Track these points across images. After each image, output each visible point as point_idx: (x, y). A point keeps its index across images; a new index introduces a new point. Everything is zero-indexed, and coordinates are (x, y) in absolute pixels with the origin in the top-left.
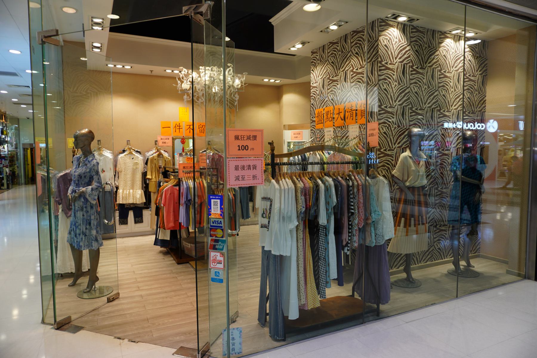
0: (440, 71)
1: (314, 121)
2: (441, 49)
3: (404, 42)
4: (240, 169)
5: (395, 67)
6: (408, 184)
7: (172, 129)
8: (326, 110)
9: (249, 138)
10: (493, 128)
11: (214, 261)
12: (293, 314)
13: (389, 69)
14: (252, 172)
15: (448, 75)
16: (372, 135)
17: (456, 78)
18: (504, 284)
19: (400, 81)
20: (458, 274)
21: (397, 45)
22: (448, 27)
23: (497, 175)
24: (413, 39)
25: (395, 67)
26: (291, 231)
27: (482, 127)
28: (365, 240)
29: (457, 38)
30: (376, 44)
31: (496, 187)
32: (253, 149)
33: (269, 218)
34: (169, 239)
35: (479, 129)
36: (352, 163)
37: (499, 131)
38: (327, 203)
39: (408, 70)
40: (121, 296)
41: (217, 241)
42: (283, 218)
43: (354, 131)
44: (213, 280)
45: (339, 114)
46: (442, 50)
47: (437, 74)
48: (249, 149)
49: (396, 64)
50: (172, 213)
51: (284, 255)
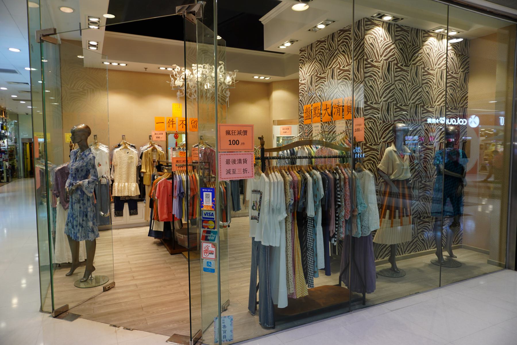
0: (424, 68)
1: (303, 117)
2: (424, 47)
3: (389, 40)
4: (231, 163)
5: (380, 64)
6: (392, 177)
7: (166, 125)
8: (314, 106)
9: (239, 133)
10: (475, 123)
11: (206, 251)
12: (282, 303)
13: (374, 66)
14: (242, 166)
15: (431, 72)
16: (358, 130)
17: (439, 75)
18: (485, 274)
19: (385, 78)
20: (440, 264)
21: (382, 43)
22: (431, 26)
23: (479, 168)
24: (398, 38)
25: (380, 64)
26: (280, 223)
27: (464, 122)
28: (351, 231)
29: (440, 37)
30: (362, 43)
31: (478, 180)
32: (244, 143)
33: (259, 210)
34: (162, 230)
35: (461, 124)
36: (339, 157)
37: (480, 126)
38: (315, 196)
39: (392, 67)
40: (116, 285)
41: (209, 232)
42: (273, 210)
43: (340, 126)
44: (205, 270)
45: (326, 109)
46: (425, 48)
47: (420, 71)
48: (240, 143)
49: (381, 62)
50: (165, 206)
51: (274, 246)
